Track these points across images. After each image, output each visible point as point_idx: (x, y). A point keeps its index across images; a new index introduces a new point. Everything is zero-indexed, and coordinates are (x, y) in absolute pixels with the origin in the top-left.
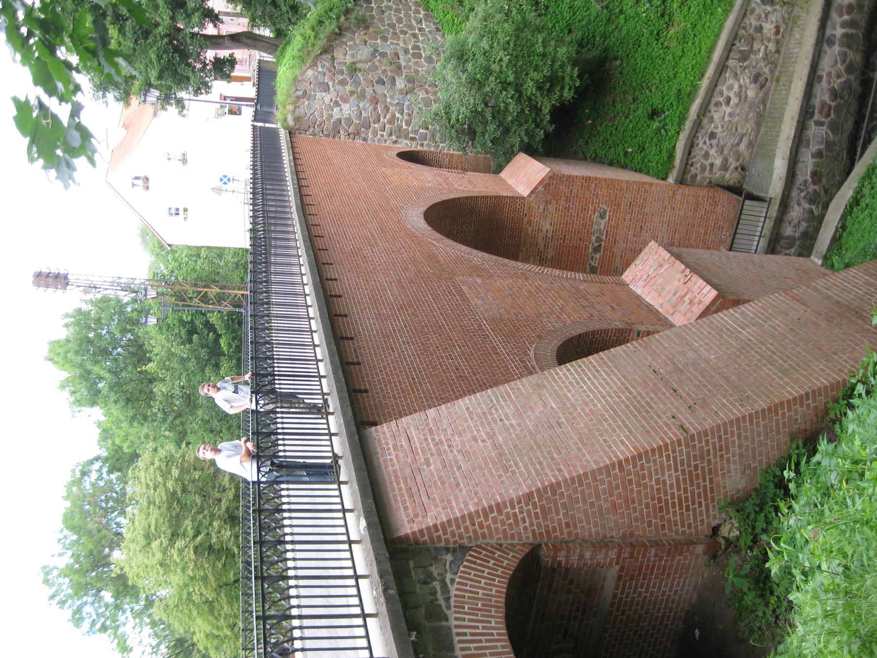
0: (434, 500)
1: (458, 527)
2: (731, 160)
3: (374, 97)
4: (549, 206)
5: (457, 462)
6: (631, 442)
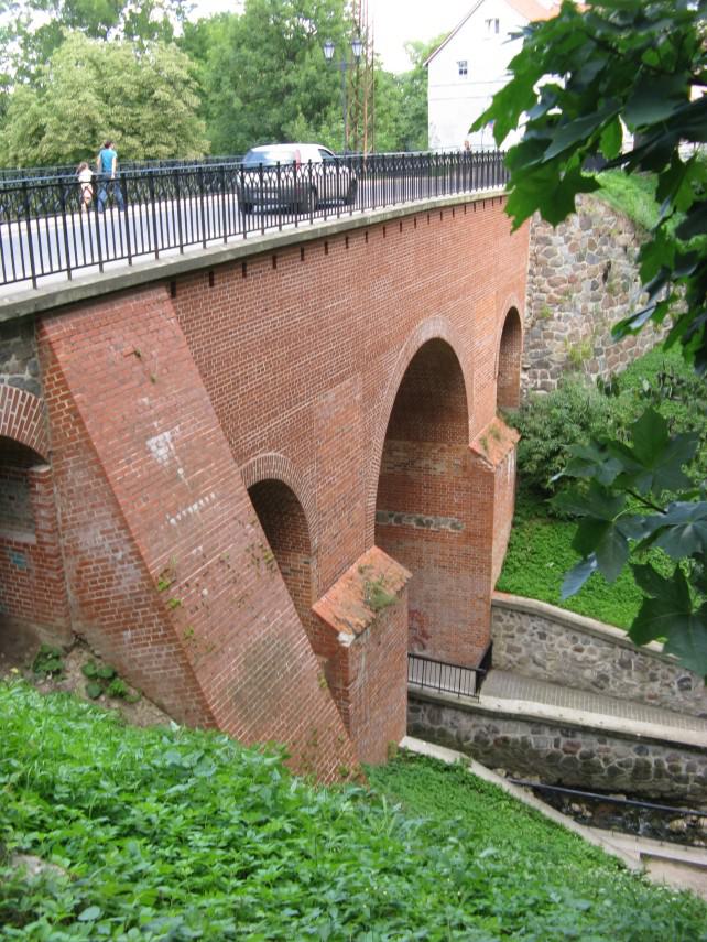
3: (576, 280)
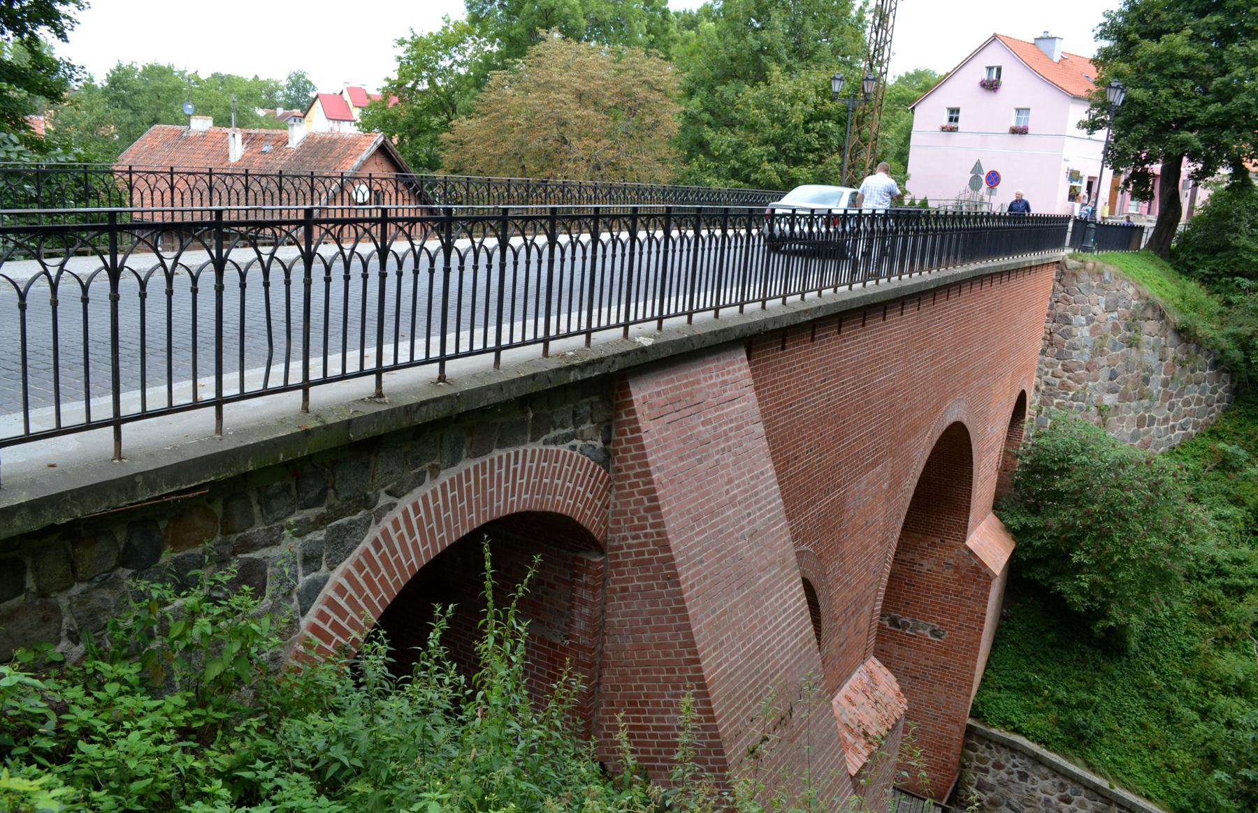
0: (667, 429)
1: (633, 458)
2: (990, 794)
4: (951, 571)
5: (706, 458)
6: (718, 676)
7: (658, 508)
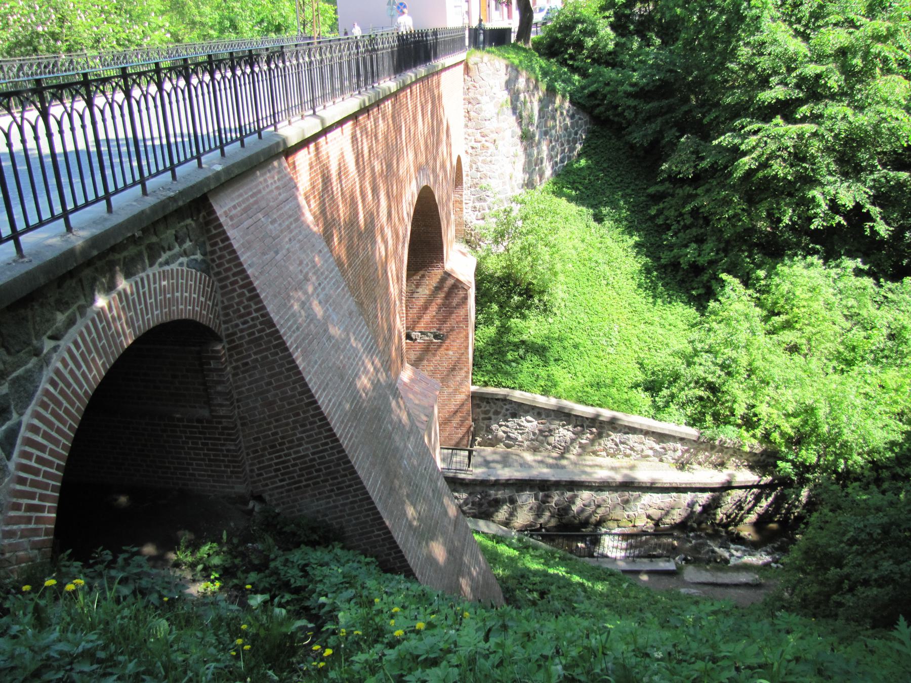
1: (229, 261)
6: (332, 409)
7: (258, 296)
